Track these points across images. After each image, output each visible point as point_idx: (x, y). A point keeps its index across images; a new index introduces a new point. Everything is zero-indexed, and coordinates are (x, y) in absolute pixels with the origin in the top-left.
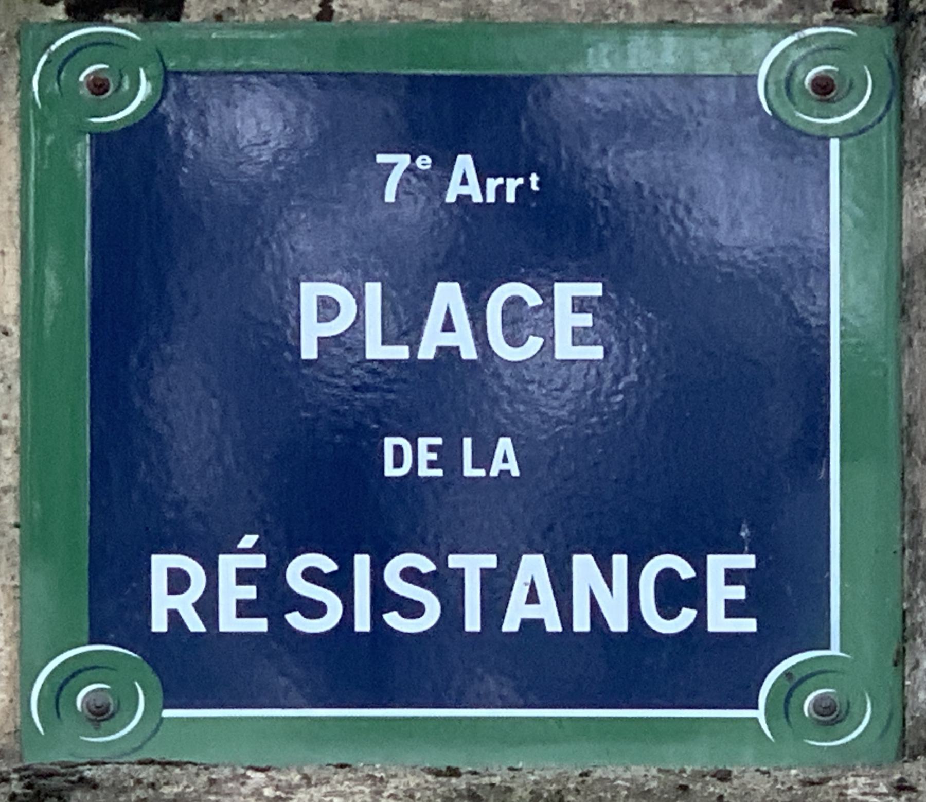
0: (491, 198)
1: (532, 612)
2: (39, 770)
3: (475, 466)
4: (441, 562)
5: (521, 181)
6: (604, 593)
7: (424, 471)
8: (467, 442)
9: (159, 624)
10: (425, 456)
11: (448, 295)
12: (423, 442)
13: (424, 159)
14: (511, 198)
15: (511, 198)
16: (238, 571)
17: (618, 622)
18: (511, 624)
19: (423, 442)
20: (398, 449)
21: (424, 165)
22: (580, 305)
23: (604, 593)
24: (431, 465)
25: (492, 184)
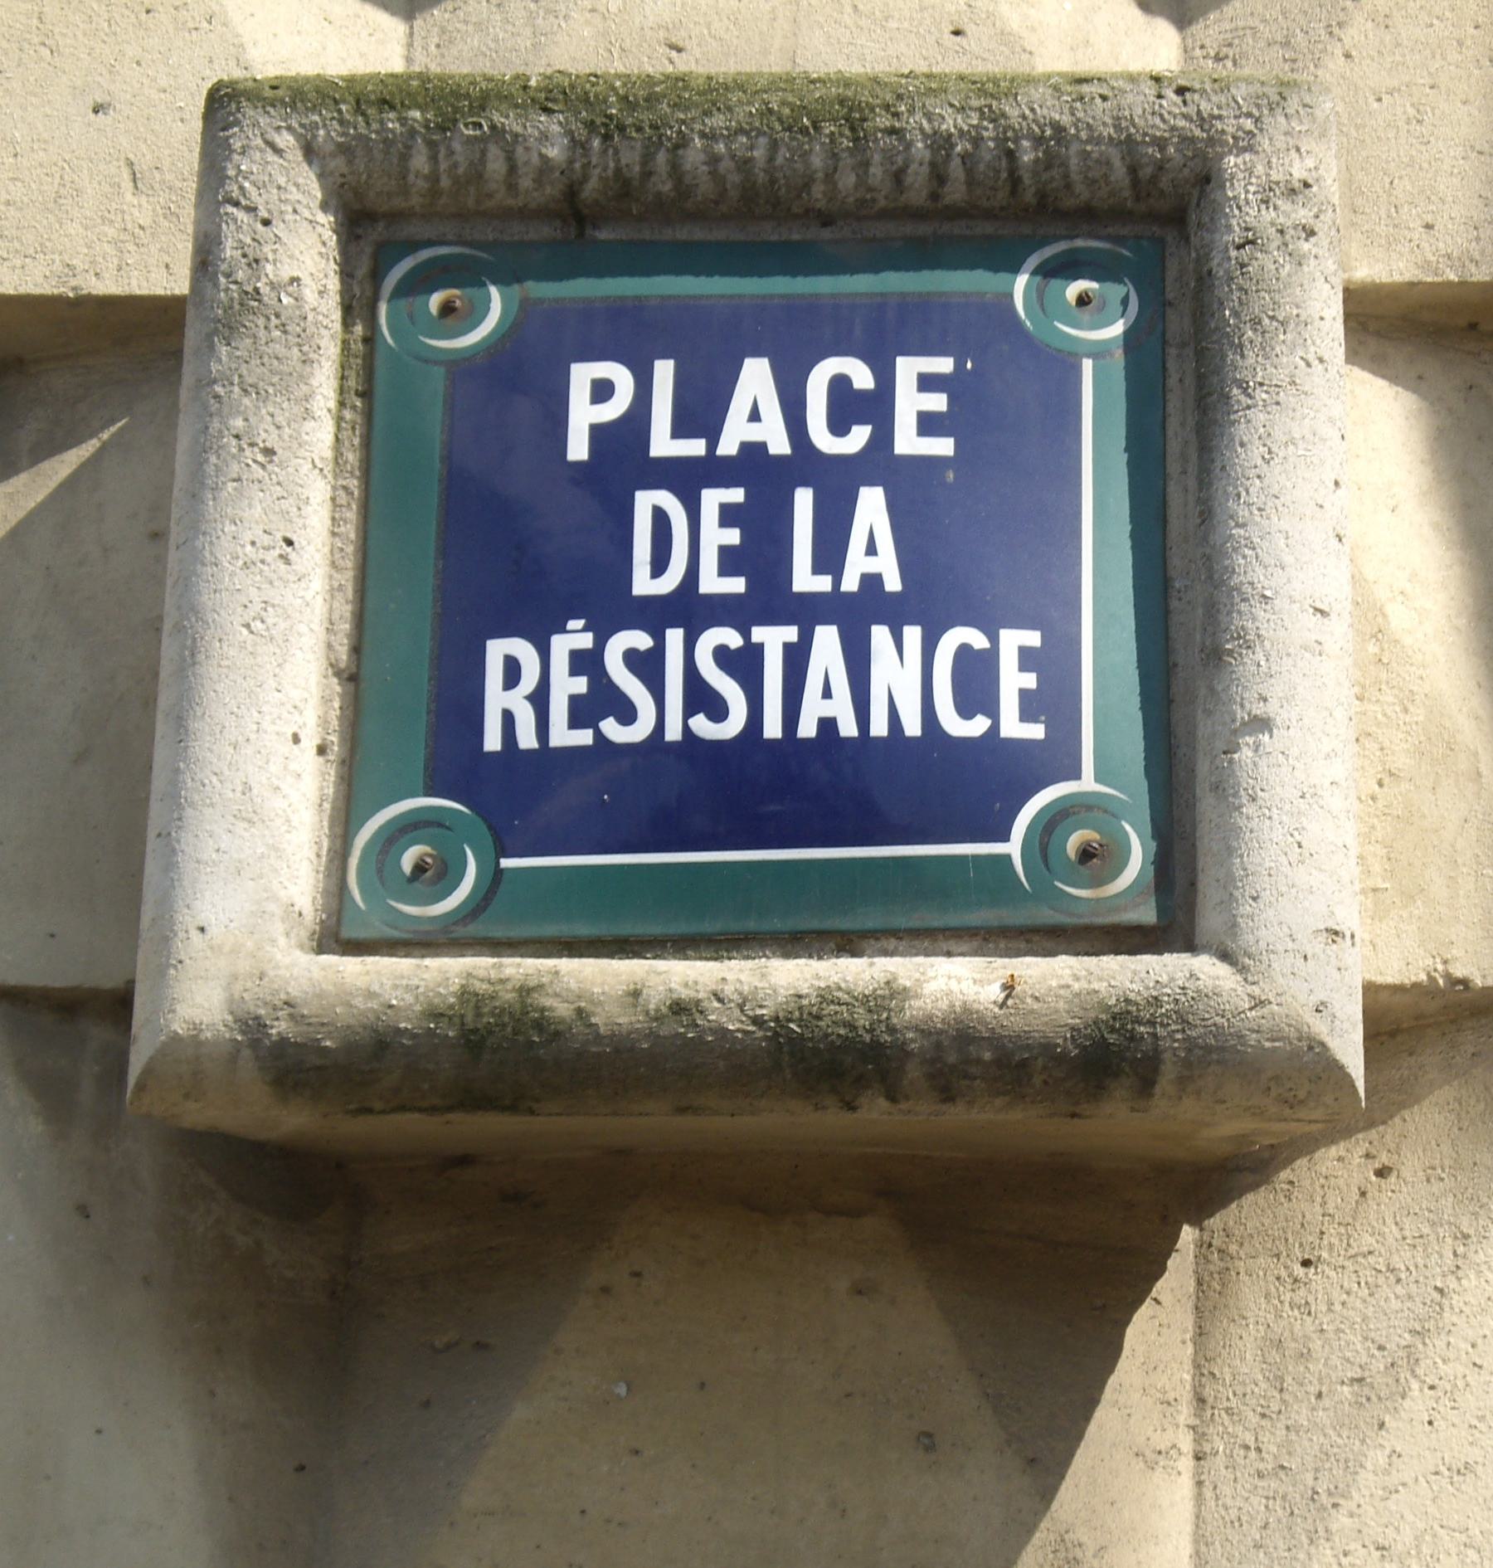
2: (1073, 74)
3: (818, 568)
4: (746, 635)
10: (717, 536)
11: (756, 379)
17: (913, 727)
18: (807, 728)
20: (661, 519)
22: (728, 516)
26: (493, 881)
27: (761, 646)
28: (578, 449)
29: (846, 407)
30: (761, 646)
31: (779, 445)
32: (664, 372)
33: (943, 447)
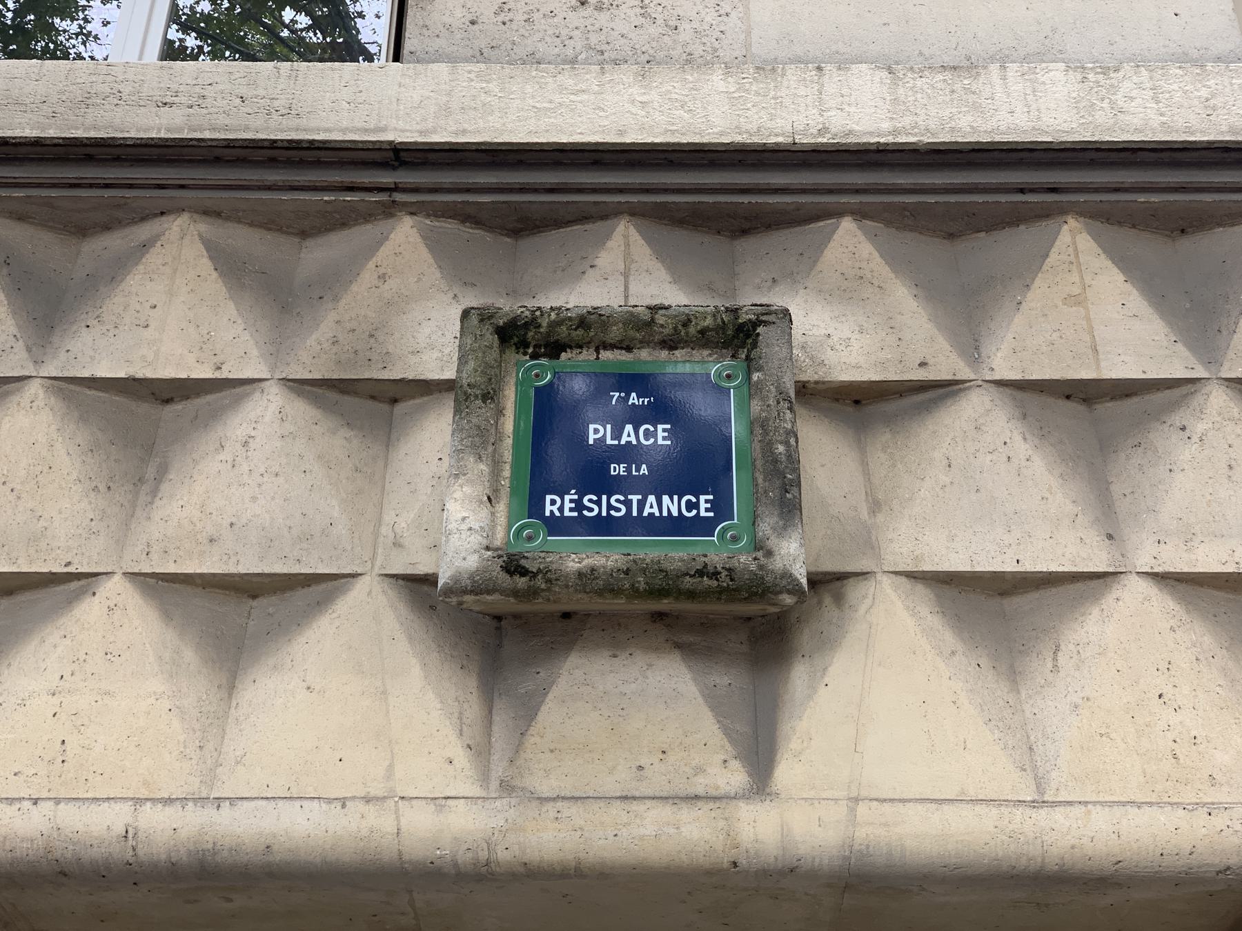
1: (651, 511)
6: (671, 506)
9: (547, 514)
11: (629, 428)
17: (675, 513)
18: (645, 514)
23: (671, 506)
26: (545, 541)
28: (591, 442)
29: (647, 434)
32: (609, 427)
33: (711, 514)
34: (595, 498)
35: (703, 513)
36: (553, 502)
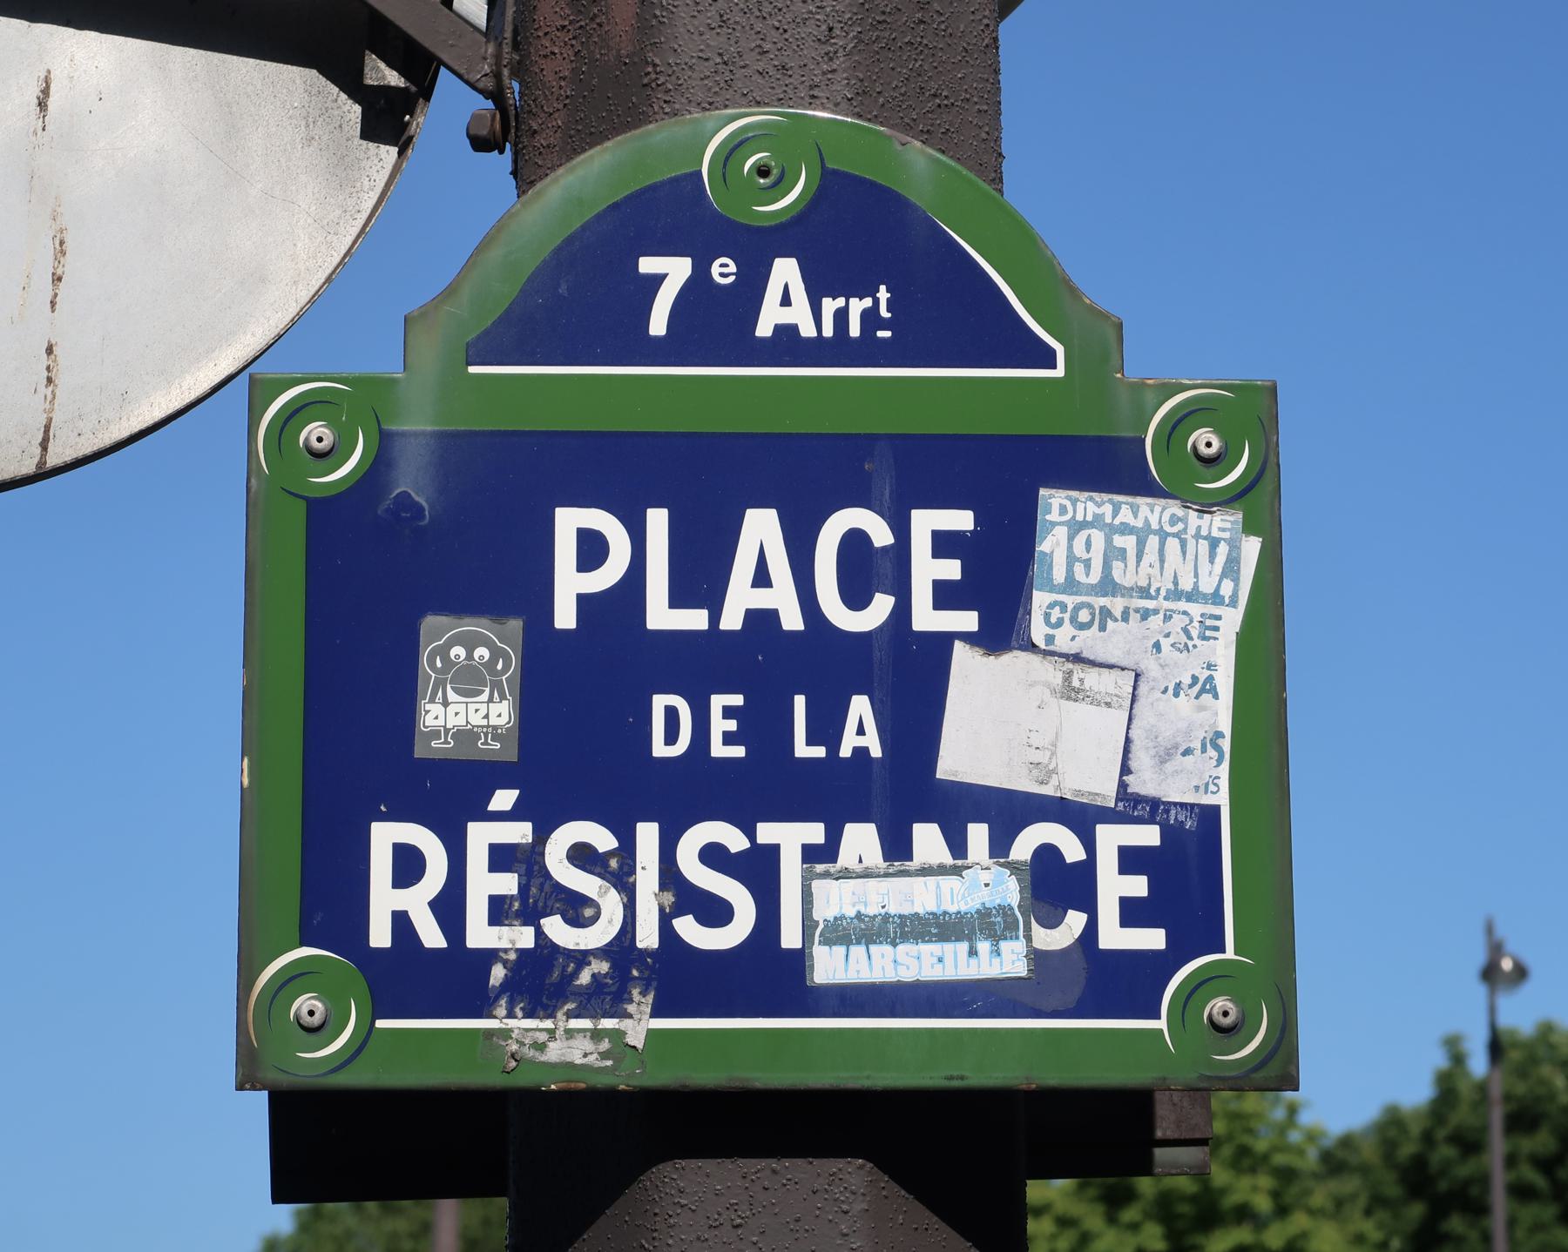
0: (828, 331)
3: (678, 599)
5: (868, 302)
7: (718, 750)
8: (800, 702)
9: (380, 936)
11: (761, 529)
12: (718, 702)
13: (726, 265)
14: (855, 330)
15: (855, 330)
16: (725, 708)
19: (718, 702)
20: (671, 714)
21: (722, 275)
24: (729, 739)
25: (830, 306)
26: (366, 1035)
27: (775, 849)
28: (565, 617)
29: (865, 570)
30: (775, 849)
31: (792, 620)
32: (657, 521)
34: (603, 839)
35: (1114, 936)
36: (408, 866)
